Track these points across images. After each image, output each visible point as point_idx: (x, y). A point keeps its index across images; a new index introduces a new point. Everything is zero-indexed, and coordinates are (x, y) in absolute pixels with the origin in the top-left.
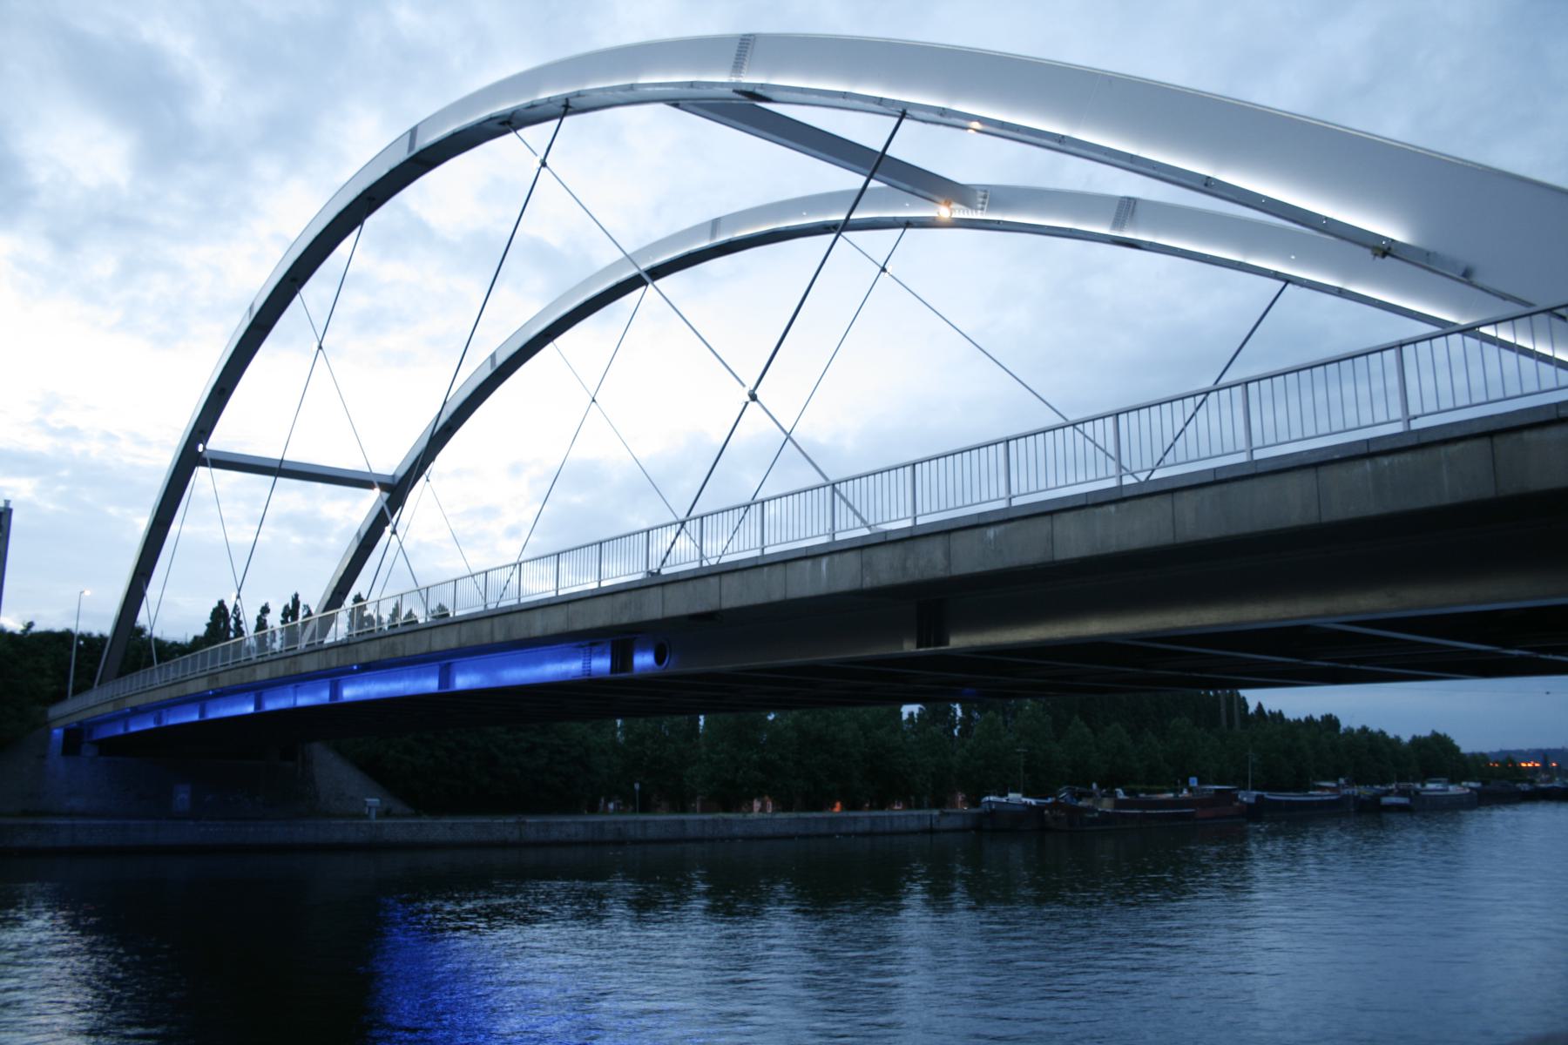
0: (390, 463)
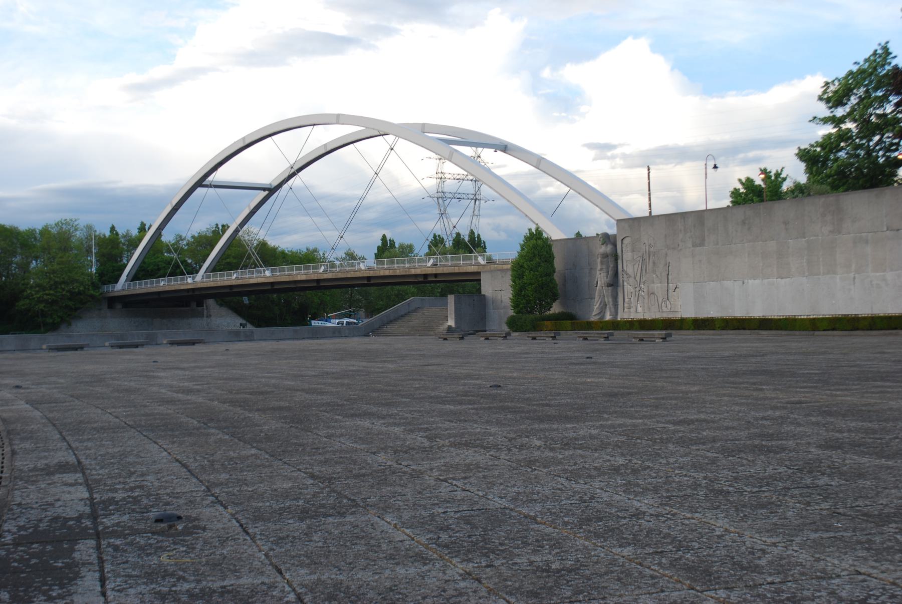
0: (200, 191)
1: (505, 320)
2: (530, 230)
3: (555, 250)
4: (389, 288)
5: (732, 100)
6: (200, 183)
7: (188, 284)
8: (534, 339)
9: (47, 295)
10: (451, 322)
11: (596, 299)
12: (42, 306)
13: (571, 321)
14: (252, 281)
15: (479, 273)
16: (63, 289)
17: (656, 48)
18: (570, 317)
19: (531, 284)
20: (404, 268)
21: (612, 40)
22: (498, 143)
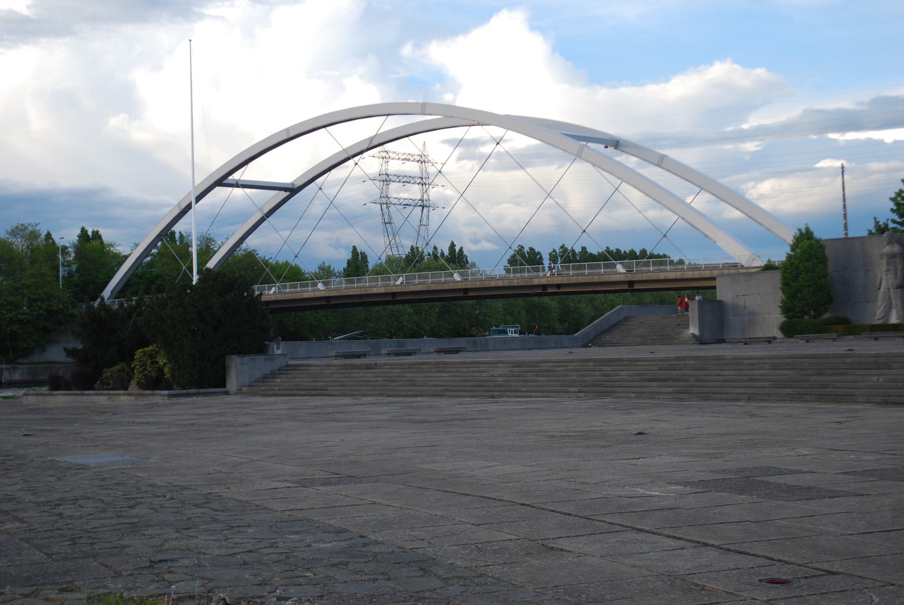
1: (779, 325)
2: (800, 230)
3: (828, 252)
4: (380, 308)
5: (628, 92)
6: (221, 182)
7: (318, 290)
8: (876, 339)
9: (21, 314)
10: (694, 330)
11: (879, 303)
12: (16, 327)
13: (848, 327)
14: (306, 295)
15: (714, 279)
16: (40, 308)
17: (535, 25)
18: (845, 321)
19: (809, 286)
20: (523, 278)
21: (483, 15)
22: (608, 138)
